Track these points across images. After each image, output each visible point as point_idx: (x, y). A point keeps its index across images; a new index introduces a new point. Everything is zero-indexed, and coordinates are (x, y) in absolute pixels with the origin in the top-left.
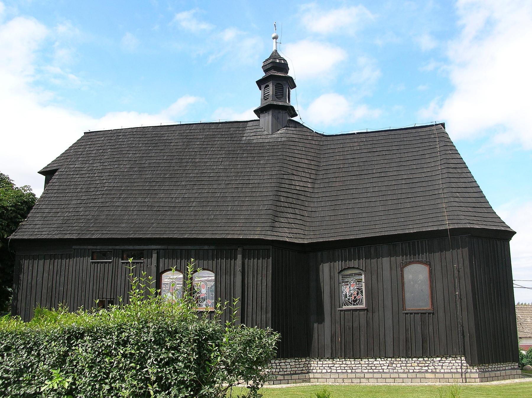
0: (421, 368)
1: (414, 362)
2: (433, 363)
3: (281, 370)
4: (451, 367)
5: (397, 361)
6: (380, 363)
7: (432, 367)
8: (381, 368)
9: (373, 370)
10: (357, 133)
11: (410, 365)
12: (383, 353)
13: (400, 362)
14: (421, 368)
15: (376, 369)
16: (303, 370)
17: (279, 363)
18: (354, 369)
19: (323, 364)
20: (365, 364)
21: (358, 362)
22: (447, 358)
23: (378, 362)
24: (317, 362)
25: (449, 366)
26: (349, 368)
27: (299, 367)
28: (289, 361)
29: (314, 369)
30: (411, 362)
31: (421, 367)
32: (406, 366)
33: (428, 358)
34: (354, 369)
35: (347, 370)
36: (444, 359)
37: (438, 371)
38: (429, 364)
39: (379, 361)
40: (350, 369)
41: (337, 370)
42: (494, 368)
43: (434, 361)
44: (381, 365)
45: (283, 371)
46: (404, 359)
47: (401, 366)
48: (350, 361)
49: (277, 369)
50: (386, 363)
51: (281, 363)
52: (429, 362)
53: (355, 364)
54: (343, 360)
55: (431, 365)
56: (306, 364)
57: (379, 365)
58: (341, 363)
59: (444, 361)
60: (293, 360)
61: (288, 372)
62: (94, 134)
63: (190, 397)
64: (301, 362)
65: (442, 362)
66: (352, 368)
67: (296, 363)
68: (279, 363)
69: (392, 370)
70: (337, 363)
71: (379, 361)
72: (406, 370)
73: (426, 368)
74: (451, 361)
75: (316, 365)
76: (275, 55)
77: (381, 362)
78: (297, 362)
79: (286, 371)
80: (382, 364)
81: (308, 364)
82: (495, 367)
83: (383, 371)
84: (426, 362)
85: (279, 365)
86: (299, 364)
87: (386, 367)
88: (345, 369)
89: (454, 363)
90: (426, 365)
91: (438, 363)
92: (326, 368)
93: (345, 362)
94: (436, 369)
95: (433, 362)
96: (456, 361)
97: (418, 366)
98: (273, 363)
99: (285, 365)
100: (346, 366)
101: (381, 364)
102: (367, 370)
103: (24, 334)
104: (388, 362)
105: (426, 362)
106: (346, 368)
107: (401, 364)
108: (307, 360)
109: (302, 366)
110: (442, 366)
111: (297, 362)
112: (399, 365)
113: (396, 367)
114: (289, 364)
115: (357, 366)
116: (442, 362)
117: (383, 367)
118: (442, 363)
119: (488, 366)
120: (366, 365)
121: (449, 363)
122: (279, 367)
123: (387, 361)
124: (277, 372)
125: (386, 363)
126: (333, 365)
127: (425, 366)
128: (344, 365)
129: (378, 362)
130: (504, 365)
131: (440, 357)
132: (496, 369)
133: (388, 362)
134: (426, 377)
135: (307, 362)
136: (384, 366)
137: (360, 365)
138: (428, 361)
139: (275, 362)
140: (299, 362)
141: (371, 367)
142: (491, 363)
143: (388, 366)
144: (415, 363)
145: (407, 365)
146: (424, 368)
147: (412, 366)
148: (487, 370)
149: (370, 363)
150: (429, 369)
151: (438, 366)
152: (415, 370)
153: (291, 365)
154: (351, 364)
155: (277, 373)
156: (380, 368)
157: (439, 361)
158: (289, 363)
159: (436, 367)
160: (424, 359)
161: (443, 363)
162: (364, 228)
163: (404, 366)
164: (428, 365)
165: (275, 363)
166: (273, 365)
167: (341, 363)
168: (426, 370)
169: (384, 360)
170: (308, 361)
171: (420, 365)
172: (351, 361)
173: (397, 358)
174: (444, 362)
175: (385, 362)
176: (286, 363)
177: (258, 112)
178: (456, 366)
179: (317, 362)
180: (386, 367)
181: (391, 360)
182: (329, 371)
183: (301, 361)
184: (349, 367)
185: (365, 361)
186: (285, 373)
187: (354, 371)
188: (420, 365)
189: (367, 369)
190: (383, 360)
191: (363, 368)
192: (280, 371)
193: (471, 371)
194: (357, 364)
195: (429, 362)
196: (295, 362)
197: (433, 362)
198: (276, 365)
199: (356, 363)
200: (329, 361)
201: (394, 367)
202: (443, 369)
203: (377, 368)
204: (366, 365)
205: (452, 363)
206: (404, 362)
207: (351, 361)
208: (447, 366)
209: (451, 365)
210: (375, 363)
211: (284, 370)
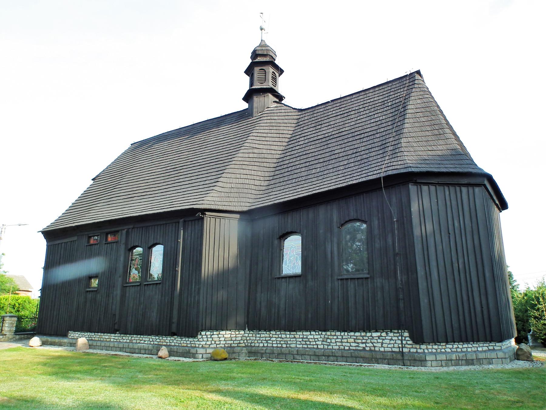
0: (358, 345)
1: (349, 337)
2: (371, 339)
4: (392, 345)
5: (332, 335)
6: (315, 337)
7: (371, 345)
8: (269, 344)
9: (350, 343)
11: (346, 340)
12: (225, 328)
13: (335, 337)
14: (358, 345)
15: (310, 344)
16: (240, 343)
18: (289, 344)
19: (260, 337)
20: (299, 338)
21: (293, 336)
22: (388, 333)
23: (312, 337)
24: (256, 335)
25: (390, 344)
26: (284, 342)
27: (236, 340)
28: (223, 332)
29: (253, 343)
30: (347, 337)
32: (342, 342)
33: (366, 333)
34: (289, 344)
35: (282, 344)
36: (384, 334)
38: (366, 340)
39: (314, 335)
40: (285, 344)
41: (273, 344)
42: (456, 348)
43: (372, 337)
44: (315, 340)
45: (215, 343)
46: (338, 333)
47: (336, 342)
48: (285, 334)
49: (208, 341)
50: (321, 337)
51: (213, 334)
52: (367, 338)
53: (290, 338)
54: (279, 333)
55: (369, 341)
56: (245, 337)
57: (314, 340)
58: (277, 336)
59: (384, 337)
61: (221, 345)
62: (144, 141)
64: (238, 334)
65: (382, 338)
66: (287, 342)
68: (211, 335)
69: (327, 346)
70: (274, 336)
71: (314, 335)
72: (342, 347)
73: (364, 345)
74: (392, 337)
75: (255, 338)
76: (263, 45)
77: (315, 337)
78: (233, 334)
79: (219, 344)
80: (316, 339)
81: (247, 337)
82: (458, 347)
83: (318, 346)
84: (363, 338)
85: (211, 337)
87: (320, 343)
88: (280, 344)
89: (396, 340)
90: (364, 341)
91: (377, 340)
92: (263, 342)
93: (281, 335)
94: (374, 347)
95: (371, 338)
96: (398, 338)
97: (355, 342)
98: (203, 335)
99: (218, 337)
100: (281, 339)
101: (315, 339)
102: (129, 349)
104: (322, 336)
105: (363, 338)
106: (281, 342)
107: (336, 339)
108: (246, 332)
109: (240, 339)
110: (382, 343)
111: (233, 334)
112: (333, 341)
113: (331, 342)
114: (223, 336)
115: (291, 340)
116: (382, 338)
117: (317, 343)
118: (381, 339)
120: (301, 340)
121: (390, 340)
123: (321, 335)
124: (208, 344)
125: (321, 337)
126: (270, 339)
127: (362, 343)
128: (279, 339)
129: (312, 337)
130: (474, 345)
131: (380, 332)
133: (322, 336)
134: (355, 359)
135: (247, 335)
136: (318, 341)
137: (294, 339)
138: (366, 336)
139: (206, 334)
140: (236, 335)
141: (305, 341)
143: (323, 341)
144: (351, 338)
145: (343, 340)
146: (361, 345)
147: (347, 342)
148: (443, 350)
149: (305, 337)
150: (366, 346)
151: (378, 343)
152: (351, 348)
153: (225, 338)
154: (286, 338)
156: (314, 343)
157: (379, 337)
158: (223, 335)
159: (375, 344)
160: (361, 334)
161: (383, 340)
162: (285, 191)
163: (339, 342)
164: (365, 341)
165: (206, 335)
166: (203, 337)
167: (277, 336)
168: (363, 347)
169: (319, 335)
170: (247, 333)
172: (286, 335)
173: (332, 332)
174: (384, 338)
175: (319, 336)
176: (220, 336)
177: (248, 98)
178: (399, 344)
179: (256, 335)
180: (320, 343)
181: (326, 335)
182: (266, 345)
183: (239, 334)
184: (285, 341)
185: (300, 335)
187: (288, 346)
189: (301, 344)
190: (317, 333)
191: (298, 343)
192: (211, 344)
193: (417, 351)
194: (292, 338)
195: (367, 338)
196: (231, 334)
197: (371, 338)
198: (207, 337)
199: (291, 337)
200: (266, 334)
201: (328, 343)
202: (383, 347)
203: (311, 344)
204: (301, 340)
205: (393, 340)
206: (339, 337)
207: (286, 335)
208: (388, 344)
209: (392, 342)
210: (310, 337)
211: (217, 342)
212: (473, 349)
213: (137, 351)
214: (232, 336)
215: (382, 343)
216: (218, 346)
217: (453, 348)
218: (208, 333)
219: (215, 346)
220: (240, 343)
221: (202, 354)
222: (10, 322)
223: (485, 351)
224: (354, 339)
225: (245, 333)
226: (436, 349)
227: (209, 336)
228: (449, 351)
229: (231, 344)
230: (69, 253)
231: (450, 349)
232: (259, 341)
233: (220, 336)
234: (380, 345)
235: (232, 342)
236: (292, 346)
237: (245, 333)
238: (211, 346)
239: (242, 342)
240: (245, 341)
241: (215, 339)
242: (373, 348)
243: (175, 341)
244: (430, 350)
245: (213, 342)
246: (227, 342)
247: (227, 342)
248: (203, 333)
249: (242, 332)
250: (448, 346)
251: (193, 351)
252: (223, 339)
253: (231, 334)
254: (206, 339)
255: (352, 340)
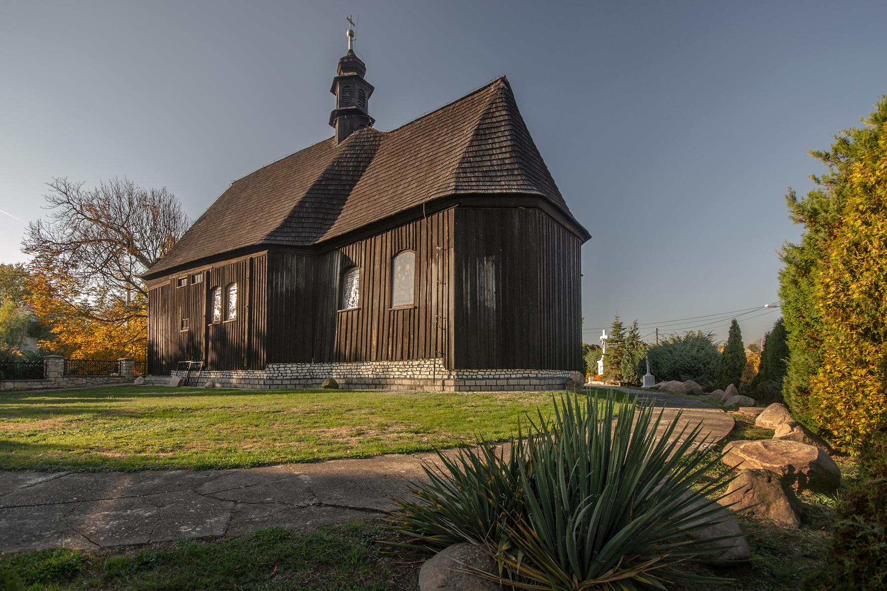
3: (280, 374)
7: (411, 373)
10: (427, 203)
16: (306, 375)
17: (278, 368)
28: (290, 366)
31: (401, 372)
37: (416, 377)
42: (488, 375)
47: (383, 372)
60: (294, 365)
61: (287, 377)
63: (370, 588)
67: (298, 369)
68: (278, 368)
77: (367, 367)
82: (490, 374)
85: (278, 370)
86: (302, 370)
94: (414, 374)
97: (398, 371)
103: (357, 530)
109: (306, 371)
110: (420, 371)
119: (477, 372)
122: (276, 372)
127: (404, 372)
130: (507, 373)
132: (492, 377)
135: (313, 368)
142: (484, 369)
146: (403, 374)
155: (275, 378)
157: (418, 365)
159: (414, 372)
161: (422, 368)
169: (370, 365)
171: (400, 370)
176: (286, 368)
180: (370, 373)
186: (284, 378)
187: (345, 376)
188: (400, 370)
192: (278, 376)
196: (297, 367)
198: (274, 370)
204: (355, 370)
211: (283, 375)
212: (506, 376)
213: (545, 387)
214: (298, 369)
215: (420, 371)
216: (284, 378)
217: (485, 375)
218: (275, 366)
219: (282, 377)
220: (306, 375)
221: (270, 385)
222: (127, 365)
223: (519, 378)
224: (398, 368)
225: (311, 366)
226: (467, 376)
227: (275, 369)
228: (481, 377)
229: (297, 376)
230: (542, 295)
231: (482, 375)
232: (323, 374)
233: (286, 368)
234: (418, 373)
235: (298, 374)
236: (348, 376)
237: (311, 366)
238: (278, 378)
239: (307, 374)
240: (311, 374)
241: (282, 372)
242: (412, 376)
243: (248, 375)
244: (460, 377)
245: (280, 374)
246: (294, 374)
247: (294, 374)
248: (270, 366)
249: (308, 365)
250: (479, 373)
251: (383, 382)
252: (289, 371)
253: (297, 367)
254: (273, 372)
255: (396, 369)
